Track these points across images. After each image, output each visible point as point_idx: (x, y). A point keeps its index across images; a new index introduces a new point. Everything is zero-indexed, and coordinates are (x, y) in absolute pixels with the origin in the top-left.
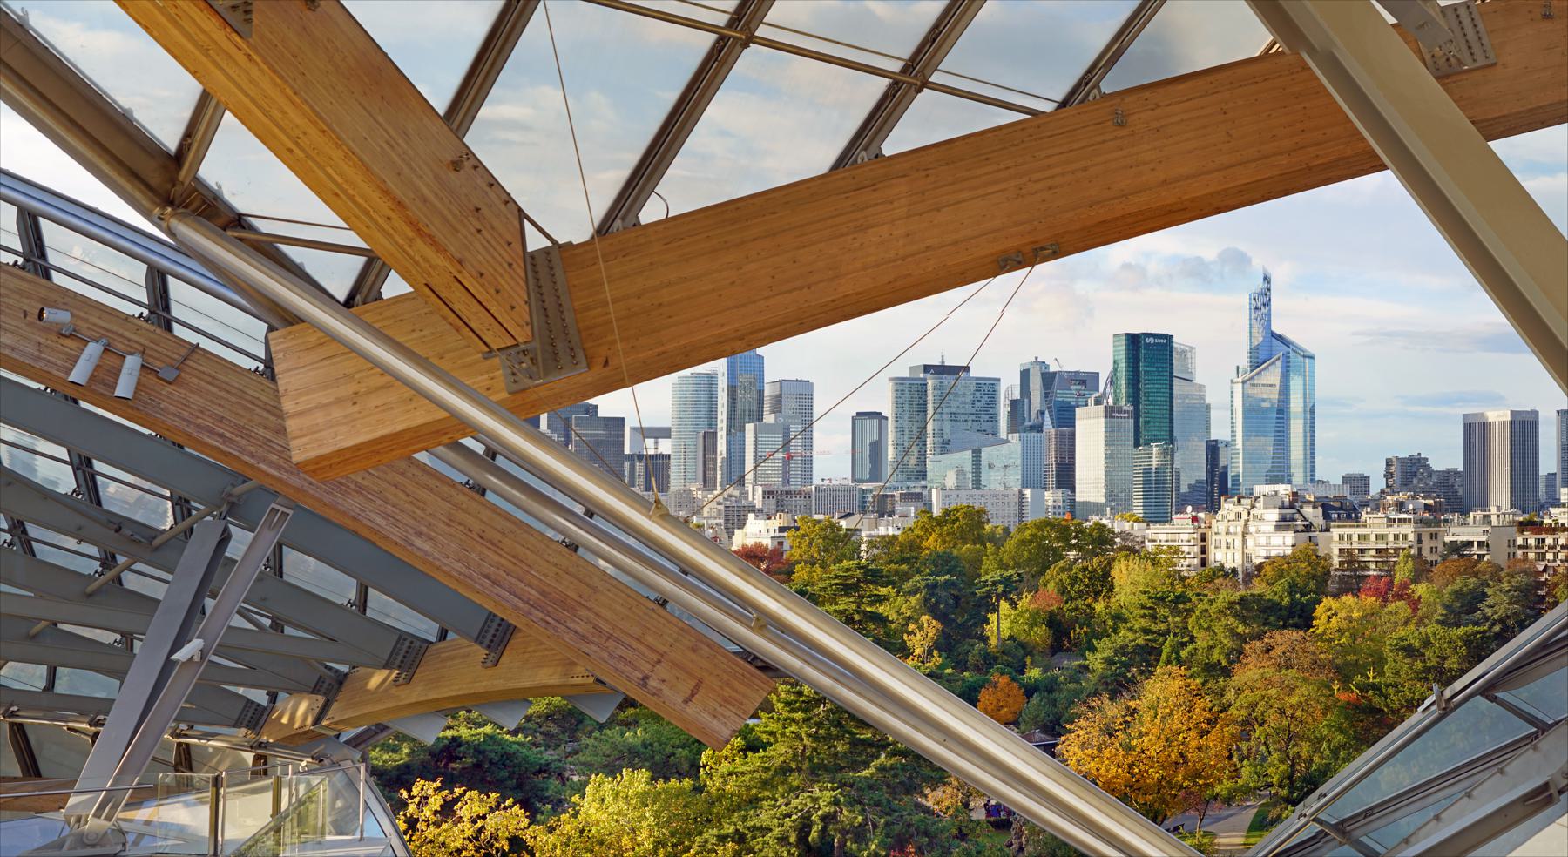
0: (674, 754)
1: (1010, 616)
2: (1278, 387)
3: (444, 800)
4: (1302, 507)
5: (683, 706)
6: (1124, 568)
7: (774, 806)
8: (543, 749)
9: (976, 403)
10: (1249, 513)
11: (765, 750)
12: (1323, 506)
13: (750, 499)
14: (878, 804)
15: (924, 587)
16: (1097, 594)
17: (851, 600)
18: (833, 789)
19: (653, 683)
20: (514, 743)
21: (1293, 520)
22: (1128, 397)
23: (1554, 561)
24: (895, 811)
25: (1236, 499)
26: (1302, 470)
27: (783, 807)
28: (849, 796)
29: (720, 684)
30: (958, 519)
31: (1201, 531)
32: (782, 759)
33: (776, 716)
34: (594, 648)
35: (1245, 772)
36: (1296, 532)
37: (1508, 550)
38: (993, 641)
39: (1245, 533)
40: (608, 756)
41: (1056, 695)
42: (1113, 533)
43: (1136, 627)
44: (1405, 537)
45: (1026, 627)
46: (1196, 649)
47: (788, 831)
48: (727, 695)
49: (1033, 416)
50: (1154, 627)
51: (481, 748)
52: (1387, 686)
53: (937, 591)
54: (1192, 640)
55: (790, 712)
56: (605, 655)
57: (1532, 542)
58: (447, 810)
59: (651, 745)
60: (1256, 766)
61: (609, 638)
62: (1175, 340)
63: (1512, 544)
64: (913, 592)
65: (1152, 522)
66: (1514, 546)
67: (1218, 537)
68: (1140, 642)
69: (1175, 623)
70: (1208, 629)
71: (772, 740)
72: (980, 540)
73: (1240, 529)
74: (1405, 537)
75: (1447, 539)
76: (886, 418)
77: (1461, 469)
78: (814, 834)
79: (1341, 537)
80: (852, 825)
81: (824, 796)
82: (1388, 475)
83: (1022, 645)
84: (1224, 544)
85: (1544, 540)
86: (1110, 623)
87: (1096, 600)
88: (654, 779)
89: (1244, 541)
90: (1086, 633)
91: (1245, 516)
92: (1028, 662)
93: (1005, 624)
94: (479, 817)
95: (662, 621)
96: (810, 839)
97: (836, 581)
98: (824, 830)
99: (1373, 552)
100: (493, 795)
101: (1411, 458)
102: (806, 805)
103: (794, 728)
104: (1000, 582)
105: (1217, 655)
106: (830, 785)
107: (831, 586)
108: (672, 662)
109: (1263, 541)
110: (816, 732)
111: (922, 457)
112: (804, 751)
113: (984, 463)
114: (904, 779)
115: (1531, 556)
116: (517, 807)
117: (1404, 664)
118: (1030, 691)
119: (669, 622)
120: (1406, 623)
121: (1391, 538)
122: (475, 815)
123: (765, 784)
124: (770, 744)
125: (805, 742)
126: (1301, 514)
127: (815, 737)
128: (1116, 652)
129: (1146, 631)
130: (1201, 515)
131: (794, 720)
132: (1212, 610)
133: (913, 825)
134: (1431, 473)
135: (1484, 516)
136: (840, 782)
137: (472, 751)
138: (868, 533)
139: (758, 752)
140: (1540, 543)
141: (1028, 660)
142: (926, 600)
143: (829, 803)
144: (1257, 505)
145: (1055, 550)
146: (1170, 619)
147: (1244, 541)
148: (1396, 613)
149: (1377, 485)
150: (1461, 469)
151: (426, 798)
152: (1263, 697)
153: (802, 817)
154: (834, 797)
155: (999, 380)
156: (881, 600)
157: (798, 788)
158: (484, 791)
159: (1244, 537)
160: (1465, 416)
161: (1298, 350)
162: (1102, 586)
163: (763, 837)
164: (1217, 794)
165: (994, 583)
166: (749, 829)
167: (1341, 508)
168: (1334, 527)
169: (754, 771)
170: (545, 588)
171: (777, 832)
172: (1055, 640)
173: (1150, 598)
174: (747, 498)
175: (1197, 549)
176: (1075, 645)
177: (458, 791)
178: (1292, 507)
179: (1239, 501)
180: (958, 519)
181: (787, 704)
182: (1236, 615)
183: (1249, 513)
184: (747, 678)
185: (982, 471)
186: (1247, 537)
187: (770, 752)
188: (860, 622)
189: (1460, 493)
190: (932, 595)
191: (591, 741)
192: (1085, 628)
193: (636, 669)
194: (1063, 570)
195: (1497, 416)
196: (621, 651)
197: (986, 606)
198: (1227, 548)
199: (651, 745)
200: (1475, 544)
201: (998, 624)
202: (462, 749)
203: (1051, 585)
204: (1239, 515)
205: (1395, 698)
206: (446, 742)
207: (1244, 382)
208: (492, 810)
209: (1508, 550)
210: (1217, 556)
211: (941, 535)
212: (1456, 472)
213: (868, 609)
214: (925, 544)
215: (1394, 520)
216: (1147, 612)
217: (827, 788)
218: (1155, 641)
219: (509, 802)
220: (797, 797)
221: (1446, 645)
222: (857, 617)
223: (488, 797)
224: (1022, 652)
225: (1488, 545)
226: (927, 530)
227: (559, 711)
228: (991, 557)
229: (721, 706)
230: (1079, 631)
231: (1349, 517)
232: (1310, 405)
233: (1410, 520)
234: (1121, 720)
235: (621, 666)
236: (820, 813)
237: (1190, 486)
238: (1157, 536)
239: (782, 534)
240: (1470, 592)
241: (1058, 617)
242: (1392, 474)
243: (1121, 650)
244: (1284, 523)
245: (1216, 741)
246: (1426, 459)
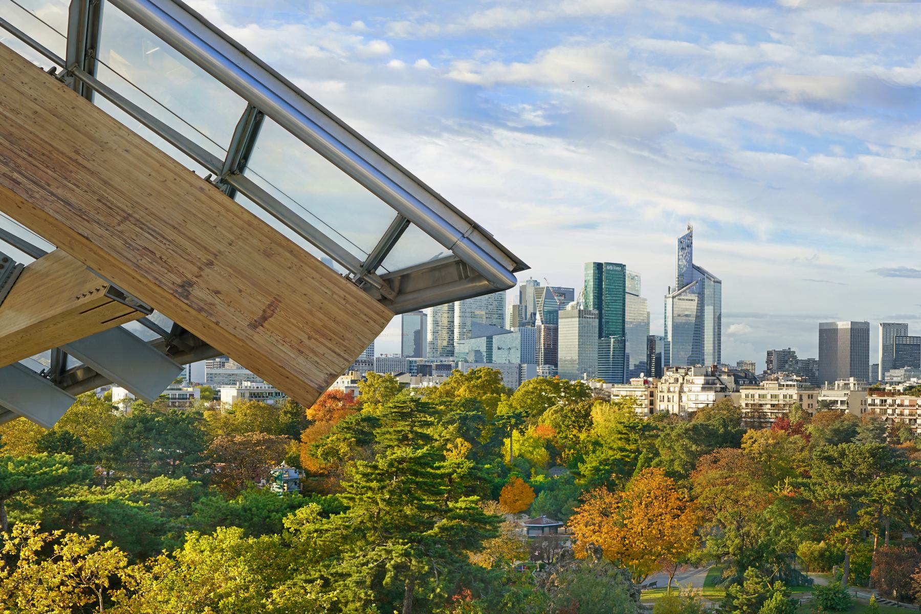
0: (269, 517)
1: (519, 441)
2: (696, 302)
3: (44, 541)
4: (720, 375)
5: (250, 331)
6: (599, 411)
7: (354, 557)
9: (490, 306)
10: (684, 379)
11: (345, 513)
12: (734, 375)
14: (442, 556)
15: (458, 419)
16: (580, 427)
17: (407, 423)
18: (404, 544)
19: (198, 293)
20: (135, 507)
21: (714, 384)
22: (594, 305)
23: (893, 415)
24: (456, 562)
25: (674, 369)
26: (712, 357)
27: (361, 558)
28: (418, 549)
29: (308, 306)
30: (480, 377)
31: (650, 390)
32: (359, 519)
33: (355, 485)
34: (98, 230)
35: (708, 544)
36: (716, 392)
37: (861, 407)
38: (508, 458)
39: (681, 391)
40: (214, 518)
41: (556, 492)
42: (590, 389)
43: (615, 446)
44: (791, 397)
45: (531, 449)
46: (661, 461)
47: (365, 577)
48: (319, 324)
49: (528, 316)
50: (628, 447)
51: (106, 510)
52: (814, 484)
53: (467, 422)
54: (657, 454)
55: (367, 482)
56: (118, 243)
57: (878, 401)
58: (46, 553)
59: (250, 509)
60: (717, 540)
61: (126, 219)
62: (627, 268)
64: (451, 422)
65: (616, 383)
67: (662, 394)
68: (618, 457)
69: (643, 444)
70: (670, 448)
71: (351, 504)
72: (498, 391)
73: (677, 389)
74: (791, 397)
75: (820, 399)
77: (817, 359)
78: (387, 579)
79: (747, 396)
80: (419, 572)
81: (397, 549)
82: (769, 362)
83: (529, 461)
84: (666, 399)
85: (886, 401)
86: (591, 448)
87: (580, 431)
88: (246, 536)
89: (680, 398)
90: (573, 454)
91: (681, 380)
92: (533, 472)
93: (516, 447)
94: (79, 556)
95: (216, 207)
96: (384, 583)
97: (395, 410)
98: (395, 578)
99: (769, 406)
100: (93, 538)
101: (784, 351)
102: (380, 556)
103: (370, 494)
104: (513, 417)
105: (677, 467)
106: (401, 541)
107: (391, 413)
108: (231, 267)
109: (693, 398)
110: (389, 498)
111: (451, 342)
112: (379, 513)
113: (495, 346)
114: (463, 537)
115: (878, 411)
116: (115, 549)
117: (826, 468)
118: (537, 489)
119: (228, 210)
120: (802, 450)
121: (781, 397)
122: (76, 556)
123: (345, 538)
124: (348, 508)
125: (381, 506)
126: (719, 380)
127: (388, 502)
128: (601, 463)
129: (622, 450)
130: (650, 379)
131: (370, 488)
132: (673, 434)
133: (471, 573)
134: (797, 362)
135: (845, 384)
136: (410, 538)
137: (97, 512)
138: (414, 386)
139: (339, 514)
140: (883, 402)
141: (533, 471)
142: (459, 429)
143: (401, 555)
144: (689, 373)
145: (549, 399)
146: (639, 442)
147: (680, 398)
148: (795, 443)
150: (817, 359)
151: (27, 539)
152: (723, 490)
153: (378, 566)
154: (406, 550)
156: (429, 424)
157: (374, 542)
158: (84, 533)
159: (680, 394)
160: (820, 324)
161: (710, 277)
162: (584, 422)
163: (344, 581)
164: (688, 559)
165: (509, 417)
166: (332, 575)
167: (746, 377)
168: (742, 389)
169: (336, 529)
170: (13, 130)
171: (355, 577)
172: (551, 459)
173: (625, 427)
175: (647, 402)
176: (565, 462)
177: (57, 533)
178: (713, 375)
179: (677, 370)
180: (480, 377)
181: (365, 475)
182: (690, 438)
183: (684, 379)
184: (352, 304)
185: (494, 351)
186: (682, 395)
187: (350, 514)
188: (413, 439)
189: (817, 374)
190: (464, 424)
191: (199, 506)
192: (572, 451)
193: (171, 270)
194: (556, 412)
195: (843, 325)
196: (145, 240)
197: (502, 433)
198: (668, 401)
199: (250, 509)
200: (839, 402)
201: (511, 446)
202: (88, 510)
203: (548, 422)
204: (677, 380)
205: (821, 493)
206: (75, 505)
207: (673, 297)
208: (92, 551)
209: (861, 407)
210: (661, 406)
211: (468, 387)
212: (814, 361)
213: (419, 430)
214: (456, 393)
215: (783, 385)
216: (623, 436)
217: (398, 543)
218: (628, 456)
219: (108, 544)
220: (373, 550)
221: (858, 456)
222: (410, 436)
223: (88, 538)
224: (528, 465)
225: (848, 403)
226: (459, 383)
227: (179, 490)
228: (504, 402)
229: (310, 338)
230: (568, 453)
231: (751, 383)
232: (718, 314)
233: (794, 385)
234: (615, 506)
235: (145, 262)
236: (392, 562)
237: (635, 366)
238: (619, 392)
239: (352, 385)
240: (845, 430)
241: (553, 443)
242: (771, 361)
243: (605, 462)
244: (707, 386)
245: (686, 522)
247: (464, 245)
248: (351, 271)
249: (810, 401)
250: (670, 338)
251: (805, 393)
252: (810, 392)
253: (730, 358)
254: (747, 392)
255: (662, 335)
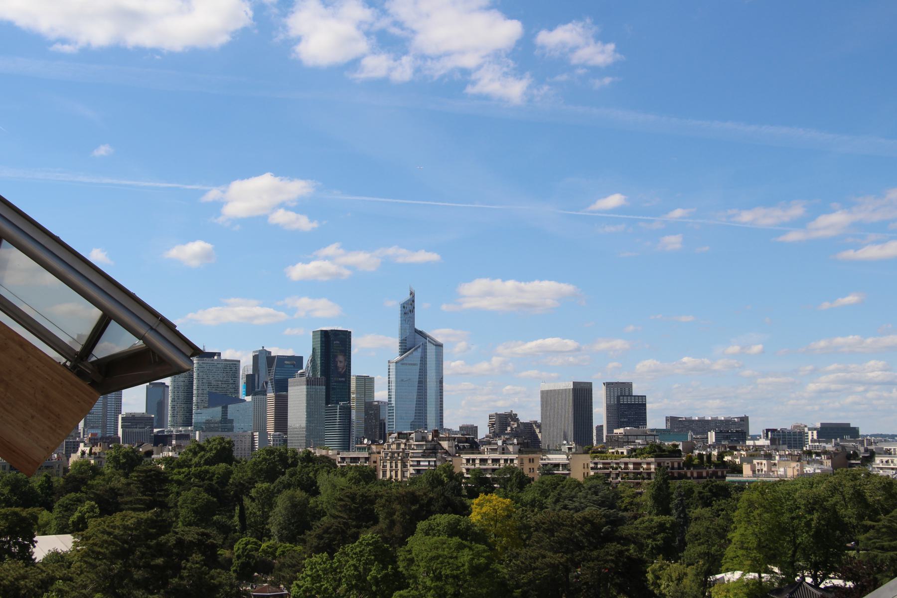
8: (195, 520)
13: (82, 437)
49: (260, 385)
63: (586, 467)
66: (588, 468)
76: (168, 387)
77: (539, 421)
149: (483, 432)
155: (239, 361)
174: (79, 437)
209: (583, 471)
212: (535, 422)
246: (516, 415)
247: (150, 336)
248: (68, 360)
249: (531, 465)
250: (393, 402)
251: (526, 457)
252: (532, 456)
253: (453, 421)
254: (468, 457)
255: (386, 400)
